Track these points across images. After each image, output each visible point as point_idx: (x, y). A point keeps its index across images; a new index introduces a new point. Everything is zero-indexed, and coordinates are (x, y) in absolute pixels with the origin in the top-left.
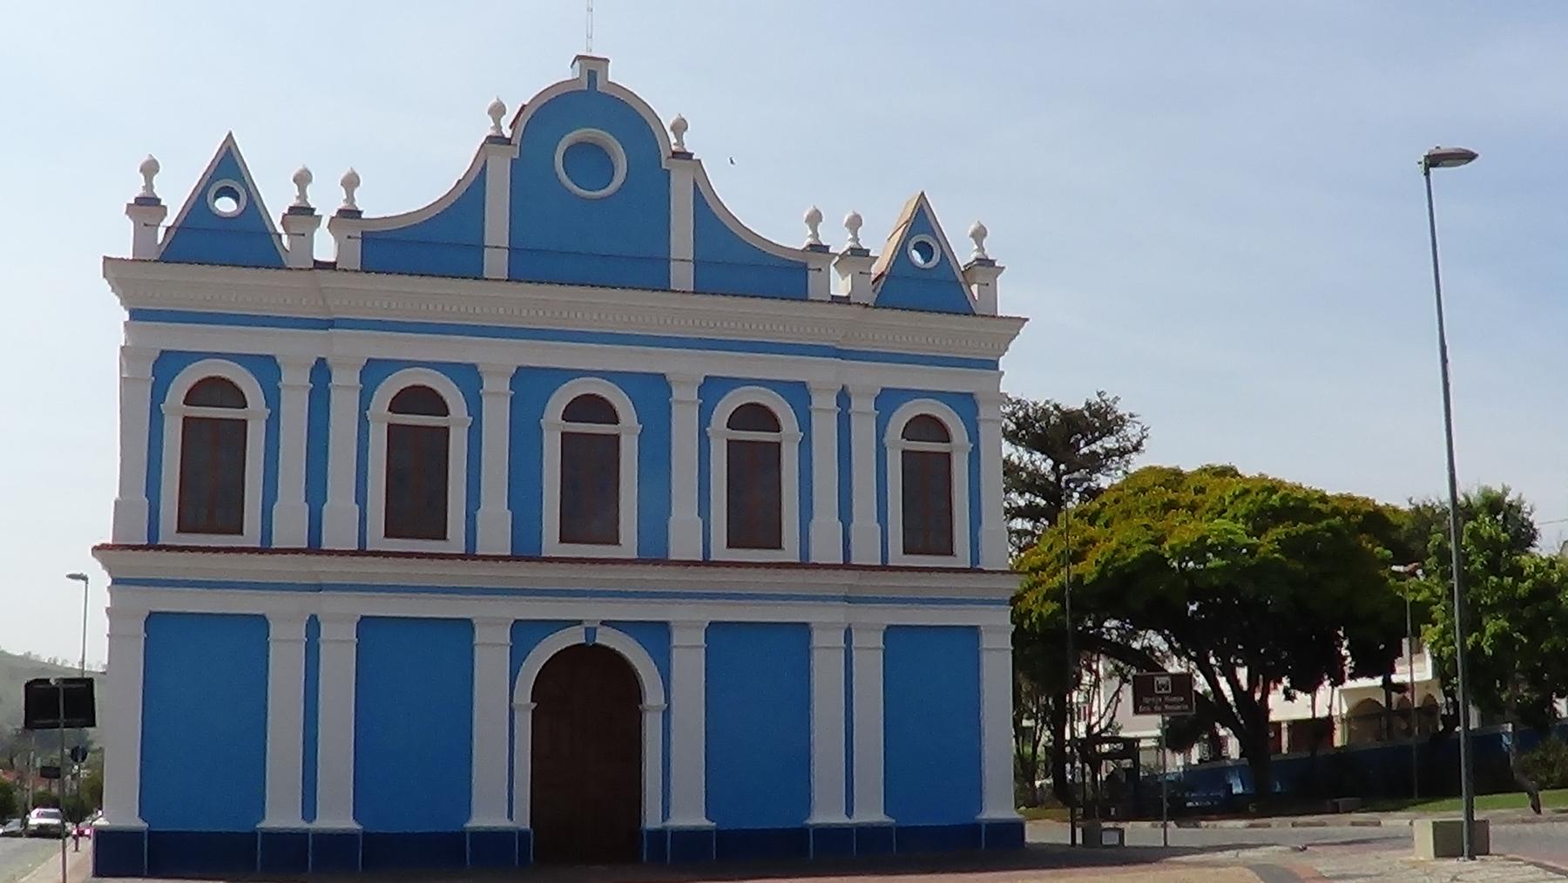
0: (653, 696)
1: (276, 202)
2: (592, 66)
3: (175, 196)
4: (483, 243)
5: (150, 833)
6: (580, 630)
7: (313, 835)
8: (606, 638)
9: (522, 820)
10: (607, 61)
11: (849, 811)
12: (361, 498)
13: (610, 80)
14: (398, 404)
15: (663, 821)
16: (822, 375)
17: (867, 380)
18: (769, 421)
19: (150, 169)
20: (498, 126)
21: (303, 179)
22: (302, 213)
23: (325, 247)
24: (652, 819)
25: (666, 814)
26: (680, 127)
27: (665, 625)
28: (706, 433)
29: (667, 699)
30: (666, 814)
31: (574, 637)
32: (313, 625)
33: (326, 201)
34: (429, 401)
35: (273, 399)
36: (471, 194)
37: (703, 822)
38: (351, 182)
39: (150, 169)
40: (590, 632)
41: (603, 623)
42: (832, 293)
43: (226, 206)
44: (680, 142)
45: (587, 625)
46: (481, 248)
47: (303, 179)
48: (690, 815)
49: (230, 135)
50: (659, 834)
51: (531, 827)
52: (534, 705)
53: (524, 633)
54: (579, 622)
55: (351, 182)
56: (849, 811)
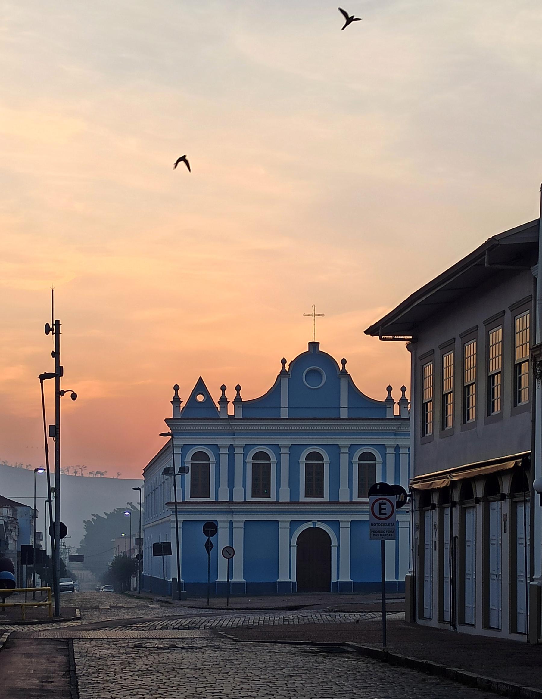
0: (334, 543)
1: (216, 396)
2: (314, 345)
3: (185, 397)
4: (340, 406)
5: (354, 583)
6: (311, 523)
7: (339, 583)
8: (319, 525)
9: (294, 579)
10: (319, 343)
11: (397, 578)
12: (244, 486)
13: (320, 350)
14: (255, 457)
15: (337, 580)
16: (224, 442)
17: (240, 442)
18: (206, 457)
19: (176, 388)
20: (284, 367)
21: (223, 388)
22: (224, 400)
23: (231, 410)
24: (334, 579)
25: (338, 578)
26: (344, 362)
27: (277, 522)
28: (245, 461)
29: (339, 543)
30: (338, 578)
31: (309, 525)
32: (231, 523)
33: (231, 395)
34: (370, 456)
35: (217, 456)
36: (275, 390)
37: (349, 580)
38: (238, 388)
39: (176, 388)
40: (314, 523)
41: (318, 521)
42: (395, 414)
43: (200, 398)
44: (344, 367)
45: (313, 521)
46: (339, 408)
47: (223, 388)
48: (345, 578)
49: (201, 377)
50: (337, 583)
51: (297, 580)
52: (297, 545)
53: (294, 524)
54: (311, 521)
55: (238, 388)
56: (397, 578)
